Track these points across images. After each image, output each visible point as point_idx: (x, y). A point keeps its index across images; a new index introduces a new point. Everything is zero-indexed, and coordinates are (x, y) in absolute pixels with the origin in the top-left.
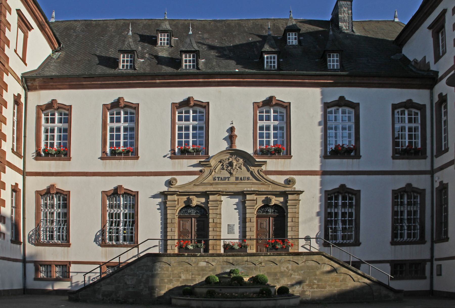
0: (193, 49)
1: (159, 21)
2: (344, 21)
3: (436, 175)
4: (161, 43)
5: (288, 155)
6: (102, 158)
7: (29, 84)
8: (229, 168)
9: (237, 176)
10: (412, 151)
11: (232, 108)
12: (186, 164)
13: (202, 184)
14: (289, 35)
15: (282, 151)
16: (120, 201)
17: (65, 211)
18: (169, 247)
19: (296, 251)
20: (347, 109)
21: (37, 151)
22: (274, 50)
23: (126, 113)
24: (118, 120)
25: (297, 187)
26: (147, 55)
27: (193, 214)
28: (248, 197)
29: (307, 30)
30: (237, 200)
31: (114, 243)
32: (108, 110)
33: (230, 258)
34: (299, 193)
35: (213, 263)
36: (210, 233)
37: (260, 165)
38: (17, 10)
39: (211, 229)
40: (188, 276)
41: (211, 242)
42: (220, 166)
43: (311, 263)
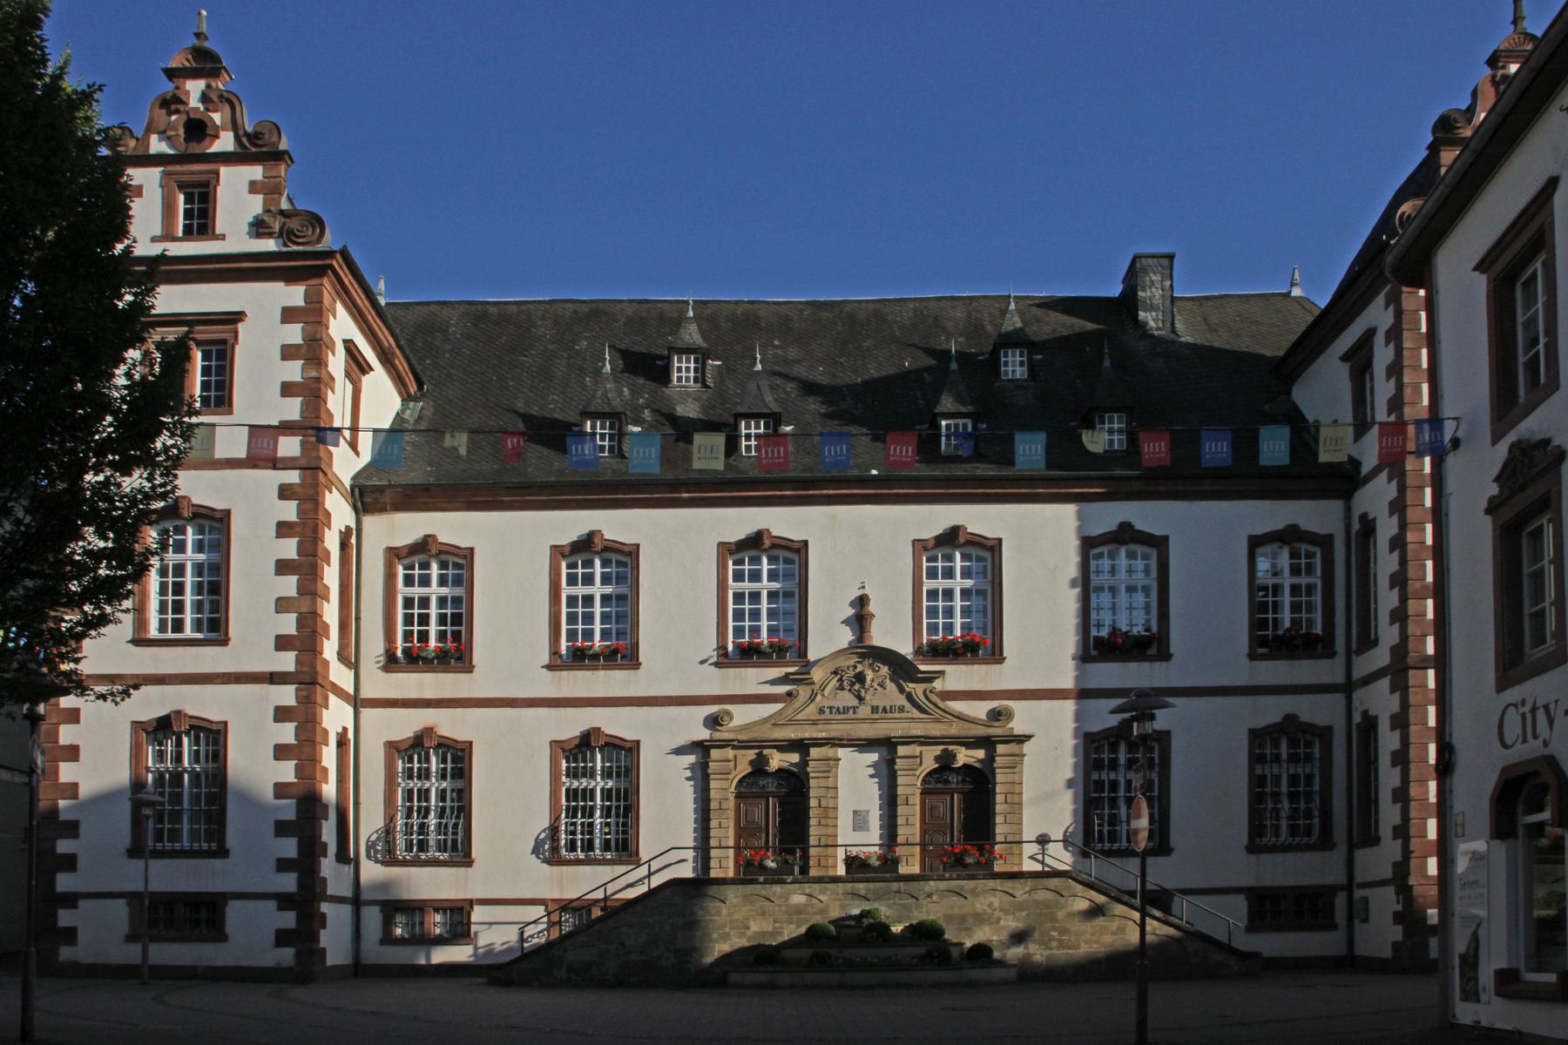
0: (766, 411)
1: (666, 307)
2: (1152, 308)
3: (1358, 695)
4: (679, 379)
5: (996, 656)
6: (550, 667)
7: (368, 500)
8: (857, 687)
9: (875, 703)
10: (1298, 642)
11: (864, 555)
12: (753, 679)
13: (792, 722)
14: (1006, 355)
15: (981, 646)
16: (593, 760)
17: (459, 784)
18: (714, 863)
19: (1016, 869)
20: (1139, 549)
21: (387, 651)
22: (964, 410)
23: (605, 564)
24: (588, 579)
25: (1018, 726)
26: (647, 414)
27: (772, 789)
28: (901, 750)
29: (1054, 330)
30: (874, 757)
31: (581, 856)
32: (564, 557)
33: (861, 885)
34: (1022, 739)
35: (822, 898)
36: (812, 831)
37: (929, 678)
38: (345, 341)
39: (813, 822)
40: (764, 924)
41: (812, 851)
42: (834, 683)
43: (1042, 895)
